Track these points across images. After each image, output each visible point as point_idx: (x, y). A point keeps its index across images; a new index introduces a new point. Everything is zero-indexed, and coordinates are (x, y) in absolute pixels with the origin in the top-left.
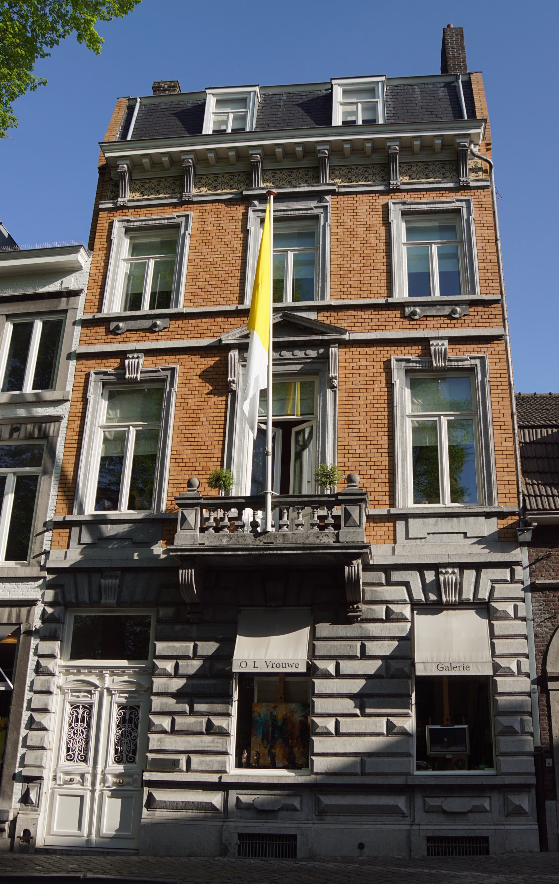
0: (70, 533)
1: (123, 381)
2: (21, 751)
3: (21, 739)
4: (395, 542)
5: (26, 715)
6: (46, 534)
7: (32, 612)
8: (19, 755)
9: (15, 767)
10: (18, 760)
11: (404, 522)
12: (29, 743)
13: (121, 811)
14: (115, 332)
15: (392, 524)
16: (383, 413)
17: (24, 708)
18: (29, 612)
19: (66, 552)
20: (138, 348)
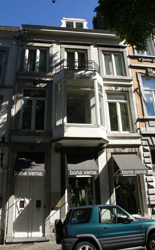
0: (145, 124)
1: (148, 76)
2: (147, 196)
3: (146, 192)
4: (146, 127)
5: (146, 184)
6: (137, 123)
7: (139, 149)
8: (147, 198)
9: (147, 202)
10: (147, 199)
11: (148, 122)
12: (150, 193)
13: (81, 162)
14: (141, 61)
15: (144, 123)
16: (139, 105)
17: (145, 182)
18: (138, 150)
19: (146, 129)
20: (150, 67)
